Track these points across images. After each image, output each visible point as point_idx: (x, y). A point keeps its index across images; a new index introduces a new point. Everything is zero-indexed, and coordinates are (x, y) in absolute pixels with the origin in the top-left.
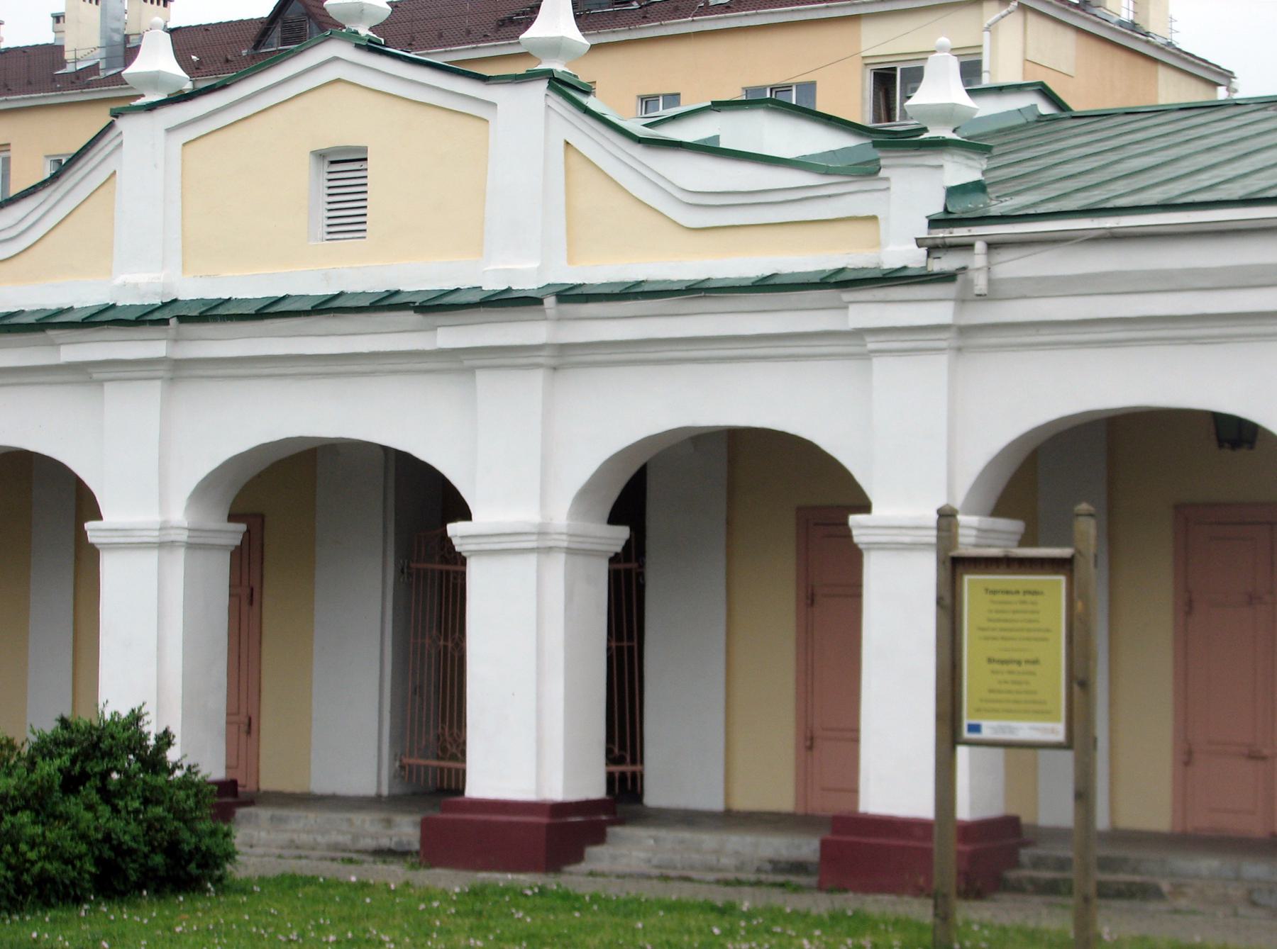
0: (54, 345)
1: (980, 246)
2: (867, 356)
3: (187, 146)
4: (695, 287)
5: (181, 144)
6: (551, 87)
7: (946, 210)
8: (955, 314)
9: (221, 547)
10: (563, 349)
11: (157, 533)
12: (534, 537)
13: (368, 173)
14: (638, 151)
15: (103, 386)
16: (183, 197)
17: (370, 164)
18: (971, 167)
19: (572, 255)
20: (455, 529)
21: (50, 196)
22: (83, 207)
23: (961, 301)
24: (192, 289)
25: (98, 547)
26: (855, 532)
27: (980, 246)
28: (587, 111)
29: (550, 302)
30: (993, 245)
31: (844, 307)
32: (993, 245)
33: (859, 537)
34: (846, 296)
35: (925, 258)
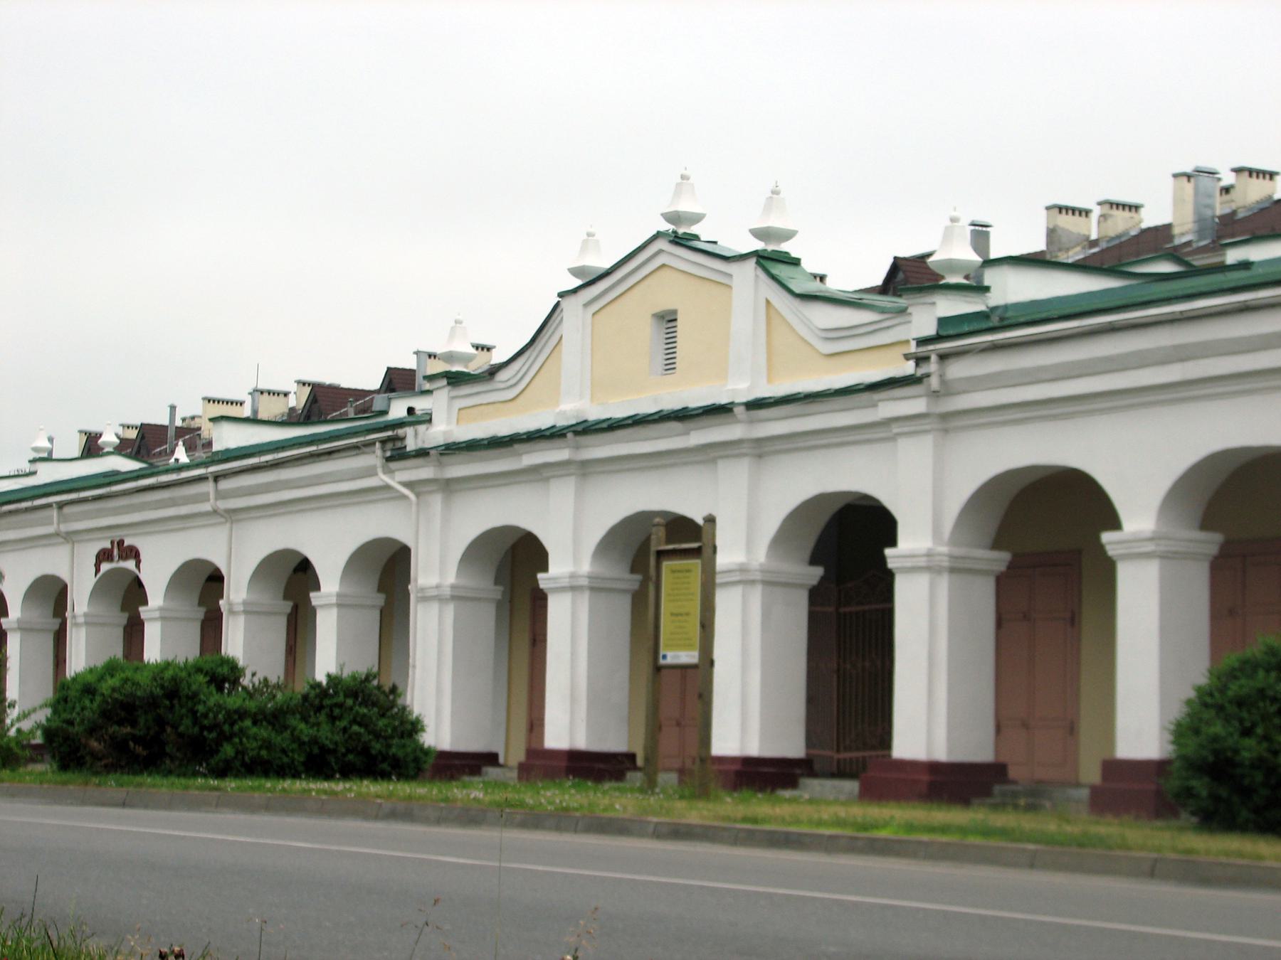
0: (687, 433)
1: (934, 358)
2: (893, 438)
3: (595, 316)
4: (855, 388)
5: (591, 315)
6: (758, 263)
7: (937, 333)
8: (928, 406)
9: (624, 591)
10: (759, 441)
11: (924, 559)
12: (738, 573)
13: (678, 329)
14: (796, 303)
15: (716, 463)
16: (592, 350)
17: (679, 323)
18: (423, 410)
19: (771, 374)
20: (1107, 537)
21: (531, 354)
22: (549, 361)
23: (935, 395)
24: (595, 413)
25: (1115, 558)
26: (141, 614)
27: (934, 358)
28: (774, 278)
29: (739, 411)
30: (943, 357)
31: (875, 405)
32: (943, 357)
33: (314, 602)
34: (876, 396)
35: (744, 400)
